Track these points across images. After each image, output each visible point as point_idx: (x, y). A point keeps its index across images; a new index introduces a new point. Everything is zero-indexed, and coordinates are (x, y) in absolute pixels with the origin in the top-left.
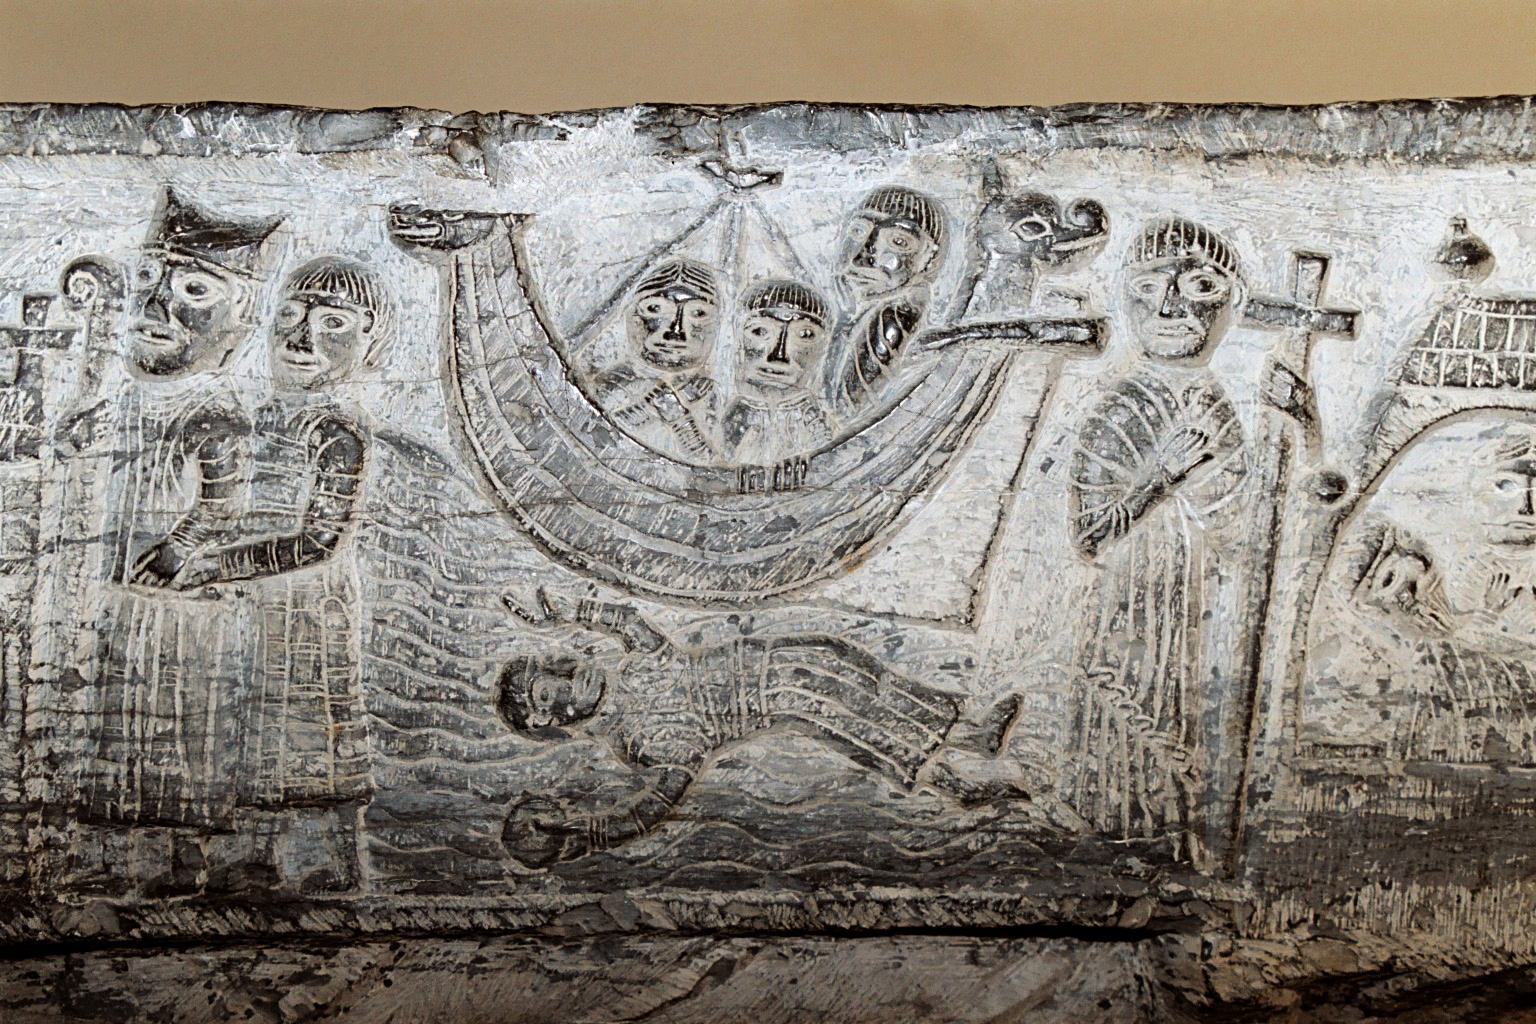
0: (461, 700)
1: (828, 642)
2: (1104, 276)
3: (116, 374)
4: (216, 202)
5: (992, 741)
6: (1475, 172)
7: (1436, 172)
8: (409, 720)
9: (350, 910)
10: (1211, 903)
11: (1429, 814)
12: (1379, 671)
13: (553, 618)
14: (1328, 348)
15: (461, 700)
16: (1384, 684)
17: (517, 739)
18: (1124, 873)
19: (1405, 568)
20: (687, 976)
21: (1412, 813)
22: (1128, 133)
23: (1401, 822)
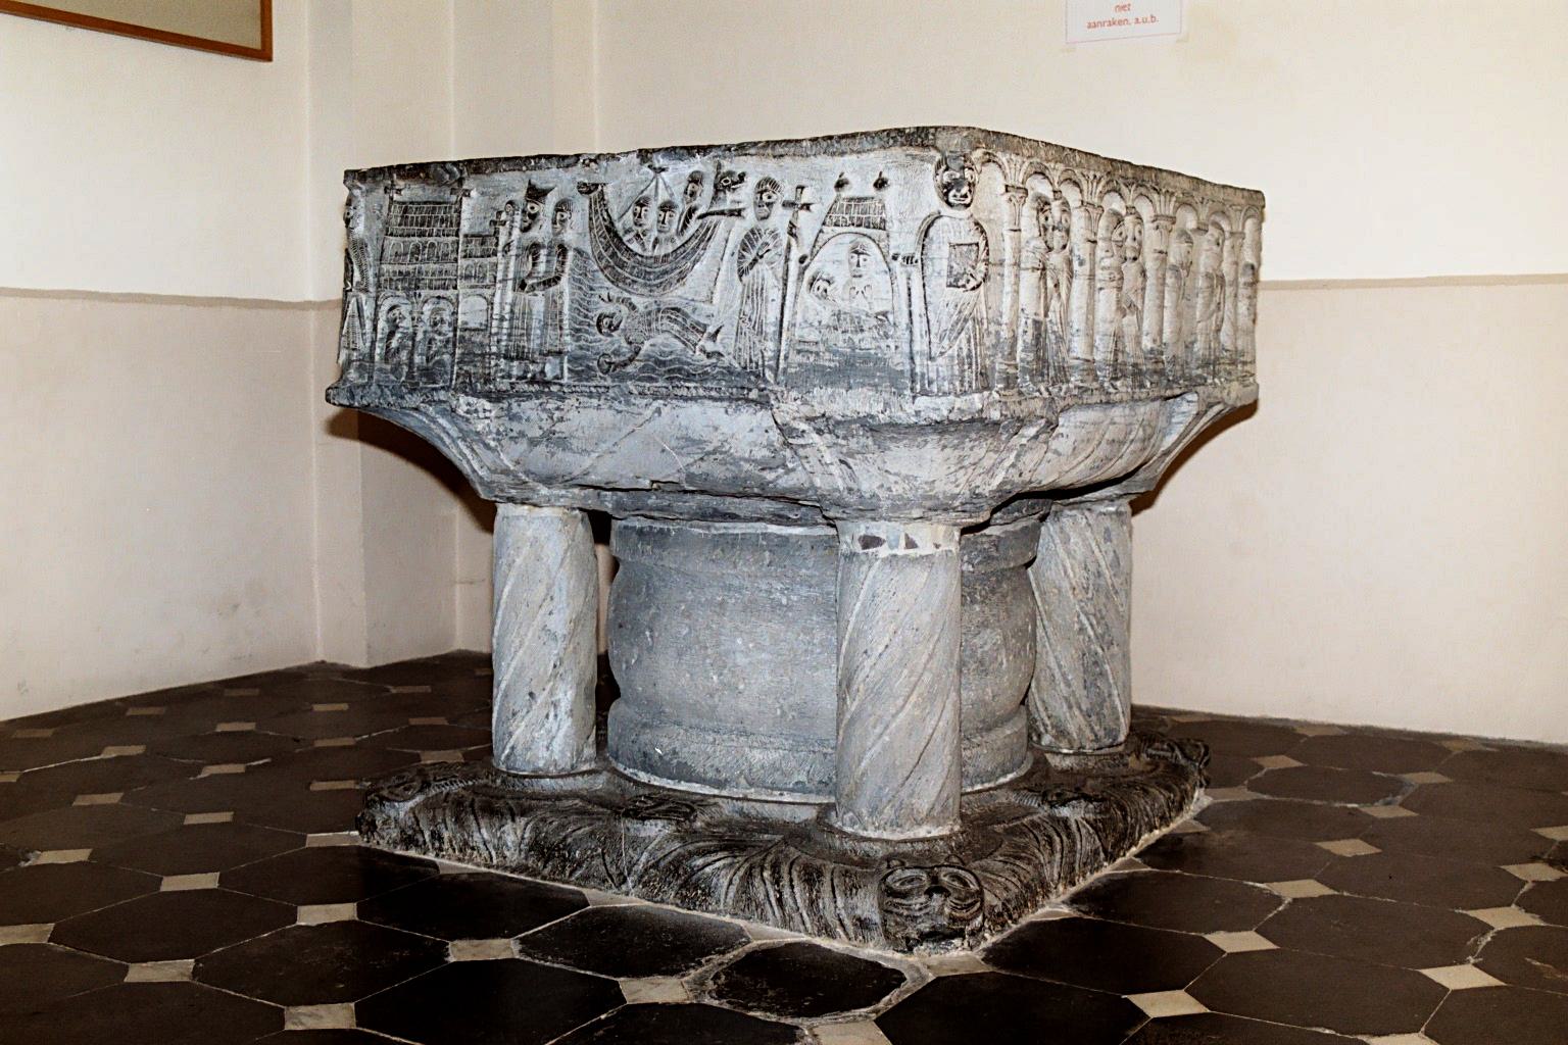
0: (589, 325)
1: (673, 309)
2: (745, 194)
3: (516, 232)
4: (540, 185)
5: (714, 337)
6: (847, 158)
7: (837, 158)
8: (578, 330)
9: (561, 385)
10: (771, 391)
11: (832, 364)
12: (818, 318)
13: (610, 300)
14: (803, 214)
15: (589, 325)
16: (820, 322)
17: (600, 336)
18: (749, 380)
19: (823, 285)
20: (648, 413)
21: (827, 364)
22: (752, 151)
23: (824, 366)
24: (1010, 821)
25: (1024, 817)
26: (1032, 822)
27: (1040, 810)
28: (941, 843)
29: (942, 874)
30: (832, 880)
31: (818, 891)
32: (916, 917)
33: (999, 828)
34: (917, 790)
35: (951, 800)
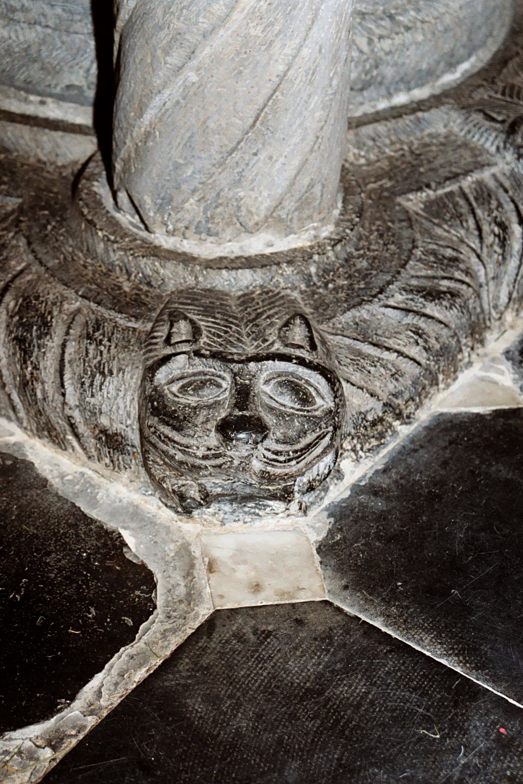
24: (440, 184)
25: (467, 173)
26: (480, 183)
27: (498, 159)
28: (288, 270)
29: (264, 376)
30: (64, 346)
31: (36, 368)
32: (199, 468)
33: (414, 202)
34: (249, 175)
35: (317, 189)
